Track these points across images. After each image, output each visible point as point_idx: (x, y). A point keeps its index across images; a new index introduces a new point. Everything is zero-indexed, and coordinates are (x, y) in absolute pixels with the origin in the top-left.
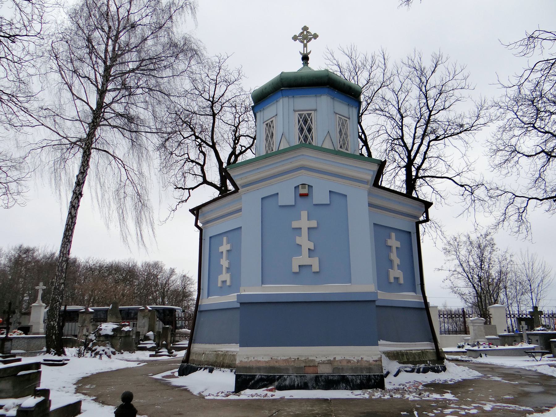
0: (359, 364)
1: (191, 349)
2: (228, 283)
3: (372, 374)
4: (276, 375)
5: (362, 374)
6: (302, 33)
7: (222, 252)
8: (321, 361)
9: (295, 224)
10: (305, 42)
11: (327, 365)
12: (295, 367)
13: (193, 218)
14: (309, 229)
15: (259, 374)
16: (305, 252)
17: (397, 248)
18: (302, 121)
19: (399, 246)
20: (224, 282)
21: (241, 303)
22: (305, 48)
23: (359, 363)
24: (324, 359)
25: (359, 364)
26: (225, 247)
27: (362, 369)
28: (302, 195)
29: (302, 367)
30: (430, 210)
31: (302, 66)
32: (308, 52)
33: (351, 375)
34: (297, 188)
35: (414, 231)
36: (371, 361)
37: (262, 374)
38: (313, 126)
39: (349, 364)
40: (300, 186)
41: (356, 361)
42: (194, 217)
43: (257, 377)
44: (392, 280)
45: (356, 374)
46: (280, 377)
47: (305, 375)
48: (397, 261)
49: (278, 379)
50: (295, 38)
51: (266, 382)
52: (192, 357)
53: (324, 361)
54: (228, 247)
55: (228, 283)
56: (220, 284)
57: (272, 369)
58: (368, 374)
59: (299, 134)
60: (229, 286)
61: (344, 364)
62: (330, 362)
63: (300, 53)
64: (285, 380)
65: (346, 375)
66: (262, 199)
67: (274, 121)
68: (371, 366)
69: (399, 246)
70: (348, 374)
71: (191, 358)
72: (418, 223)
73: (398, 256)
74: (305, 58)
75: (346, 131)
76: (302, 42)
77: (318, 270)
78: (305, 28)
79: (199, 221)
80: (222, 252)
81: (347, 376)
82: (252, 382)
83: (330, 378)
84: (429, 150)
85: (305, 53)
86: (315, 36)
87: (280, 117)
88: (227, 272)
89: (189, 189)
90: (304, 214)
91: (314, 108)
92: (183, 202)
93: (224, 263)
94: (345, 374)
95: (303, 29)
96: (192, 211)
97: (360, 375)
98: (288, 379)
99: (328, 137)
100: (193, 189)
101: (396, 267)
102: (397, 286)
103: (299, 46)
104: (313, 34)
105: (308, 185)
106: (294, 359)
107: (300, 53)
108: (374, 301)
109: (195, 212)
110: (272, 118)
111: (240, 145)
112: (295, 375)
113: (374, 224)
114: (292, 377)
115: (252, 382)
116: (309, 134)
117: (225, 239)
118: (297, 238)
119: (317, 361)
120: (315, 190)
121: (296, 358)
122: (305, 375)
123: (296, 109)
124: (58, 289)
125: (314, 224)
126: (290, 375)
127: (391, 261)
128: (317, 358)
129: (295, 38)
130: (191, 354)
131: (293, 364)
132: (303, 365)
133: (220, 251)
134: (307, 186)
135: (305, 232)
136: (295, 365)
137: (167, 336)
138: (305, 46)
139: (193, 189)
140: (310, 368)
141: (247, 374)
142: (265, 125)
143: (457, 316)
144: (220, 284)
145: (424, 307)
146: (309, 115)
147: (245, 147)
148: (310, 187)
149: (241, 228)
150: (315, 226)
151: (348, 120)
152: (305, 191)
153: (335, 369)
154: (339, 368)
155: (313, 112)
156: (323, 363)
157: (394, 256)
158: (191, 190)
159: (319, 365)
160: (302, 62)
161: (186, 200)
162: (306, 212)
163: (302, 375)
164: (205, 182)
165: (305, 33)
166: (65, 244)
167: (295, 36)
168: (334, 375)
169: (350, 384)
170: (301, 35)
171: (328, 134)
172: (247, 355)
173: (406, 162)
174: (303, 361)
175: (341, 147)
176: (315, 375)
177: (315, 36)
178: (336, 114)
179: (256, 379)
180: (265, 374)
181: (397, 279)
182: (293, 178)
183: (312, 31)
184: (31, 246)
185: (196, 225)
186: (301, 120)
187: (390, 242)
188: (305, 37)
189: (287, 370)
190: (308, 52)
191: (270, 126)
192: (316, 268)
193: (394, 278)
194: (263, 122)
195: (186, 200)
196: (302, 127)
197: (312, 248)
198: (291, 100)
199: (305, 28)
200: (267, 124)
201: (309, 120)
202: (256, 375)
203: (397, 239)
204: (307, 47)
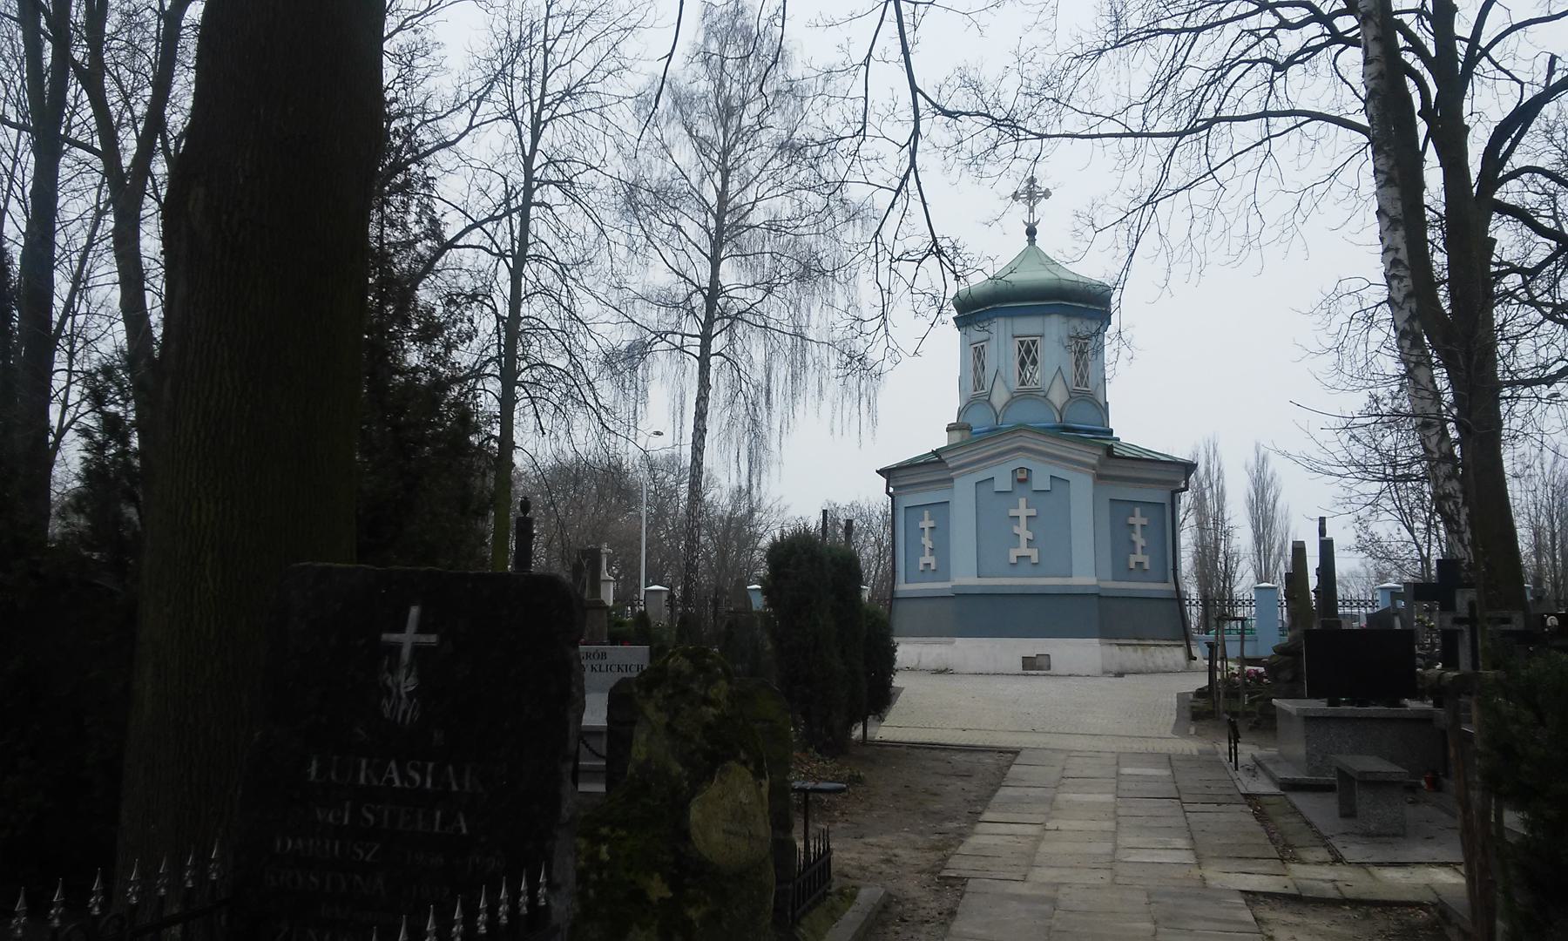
2: (933, 567)
9: (1013, 513)
16: (1024, 543)
22: (1031, 214)
26: (926, 524)
28: (1020, 481)
34: (1014, 471)
35: (1167, 501)
38: (1038, 359)
48: (1140, 541)
54: (932, 524)
55: (933, 567)
56: (921, 568)
60: (935, 570)
66: (976, 483)
77: (1037, 561)
85: (1031, 222)
90: (1022, 502)
93: (927, 542)
99: (1059, 376)
101: (1139, 550)
102: (1140, 571)
103: (1021, 208)
117: (926, 513)
123: (1016, 333)
124: (692, 565)
125: (1033, 512)
127: (1133, 543)
133: (921, 527)
135: (1023, 521)
138: (1031, 210)
143: (1347, 604)
145: (1176, 597)
146: (1034, 342)
149: (948, 502)
150: (1035, 514)
152: (1023, 476)
162: (1024, 499)
166: (694, 504)
171: (1059, 372)
175: (1077, 385)
181: (1139, 564)
185: (888, 492)
187: (1131, 520)
192: (1035, 559)
193: (1136, 563)
197: (1031, 538)
198: (1009, 321)
203: (1142, 516)
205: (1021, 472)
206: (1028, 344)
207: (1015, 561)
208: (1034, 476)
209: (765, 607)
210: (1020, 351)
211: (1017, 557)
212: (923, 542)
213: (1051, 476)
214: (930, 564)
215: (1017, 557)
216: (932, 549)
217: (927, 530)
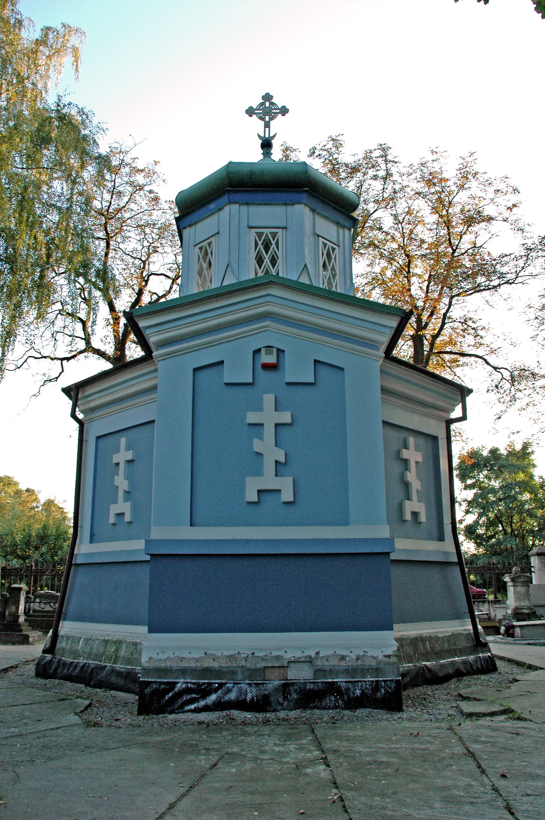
0: (360, 662)
1: (59, 629)
2: (127, 518)
3: (382, 679)
4: (213, 683)
5: (364, 680)
6: (262, 104)
7: (117, 464)
8: (293, 659)
9: (252, 417)
10: (267, 118)
11: (305, 664)
12: (249, 669)
13: (68, 403)
14: (277, 425)
15: (182, 680)
16: (269, 467)
17: (417, 463)
18: (262, 244)
19: (420, 459)
20: (121, 515)
21: (152, 555)
22: (267, 129)
23: (359, 661)
24: (298, 654)
25: (360, 662)
27: (364, 671)
28: (267, 367)
29: (260, 669)
30: (469, 399)
31: (262, 157)
32: (271, 136)
33: (345, 682)
34: (257, 352)
36: (380, 657)
37: (188, 680)
39: (343, 663)
40: (263, 351)
41: (355, 658)
42: (71, 402)
43: (179, 685)
44: (408, 517)
45: (355, 680)
46: (221, 685)
47: (265, 682)
49: (216, 690)
50: (250, 112)
51: (194, 696)
52: (61, 644)
53: (300, 658)
54: (129, 455)
55: (127, 518)
56: (112, 520)
57: (207, 672)
58: (375, 679)
59: (255, 267)
60: (130, 523)
61: (334, 662)
62: (310, 661)
63: (259, 136)
64: (229, 691)
65: (337, 682)
66: (195, 370)
67: (213, 244)
68: (380, 666)
69: (420, 459)
70: (340, 680)
71: (58, 646)
72: (450, 422)
73: (419, 477)
74: (267, 145)
75: (333, 266)
76: (262, 119)
77: (291, 499)
78: (267, 97)
79: (77, 409)
80: (117, 464)
81: (339, 684)
82: (170, 694)
83: (308, 688)
84: (450, 311)
85: (267, 136)
86: (284, 111)
87: (224, 235)
88: (126, 500)
89: (62, 360)
90: (269, 400)
91: (283, 224)
92: (50, 380)
94: (335, 680)
95: (263, 98)
96: (67, 391)
97: (360, 681)
98: (235, 689)
100: (68, 359)
104: (280, 107)
105: (278, 350)
106: (246, 655)
107: (259, 136)
108: (388, 553)
109: (72, 394)
110: (208, 238)
111: (150, 292)
112: (247, 682)
113: (384, 422)
114: (242, 685)
115: (170, 694)
116: (273, 267)
118: (256, 441)
119: (286, 658)
120: (287, 357)
121: (250, 653)
122: (265, 682)
123: (251, 224)
125: (286, 417)
126: (238, 682)
127: (407, 485)
128: (286, 652)
129: (250, 112)
130: (59, 638)
131: (243, 663)
132: (261, 665)
133: (115, 461)
134: (275, 350)
135: (269, 431)
136: (248, 666)
137: (19, 601)
138: (267, 125)
139: (68, 359)
140: (273, 670)
141: (161, 680)
142: (198, 250)
144: (112, 520)
146: (274, 235)
147: (157, 295)
148: (280, 352)
150: (289, 420)
151: (337, 247)
152: (271, 359)
153: (319, 672)
154: (325, 670)
155: (280, 231)
156: (298, 662)
157: (411, 477)
158: (65, 362)
159: (291, 664)
160: (262, 152)
161: (57, 378)
163: (259, 682)
164: (89, 348)
165: (267, 104)
167: (251, 108)
168: (315, 682)
169: (344, 697)
170: (260, 106)
172: (161, 648)
173: (415, 327)
174: (262, 659)
176: (283, 682)
177: (284, 111)
178: (318, 236)
179: (176, 689)
180: (193, 681)
181: (415, 514)
182: (251, 335)
183: (279, 101)
184: (18, 481)
185: (73, 415)
186: (260, 243)
187: (405, 454)
188: (267, 111)
189: (232, 673)
190: (271, 136)
191: (206, 251)
192: (287, 496)
194: (194, 245)
195: (57, 378)
196: (260, 256)
197: (283, 460)
199: (267, 97)
200: (201, 248)
201: (274, 243)
202: (177, 683)
203: (417, 449)
204: (269, 127)
205: (267, 353)
206: (267, 234)
207: (255, 499)
208: (288, 359)
209: (477, 534)
210: (256, 244)
211: (259, 491)
212: (116, 483)
213: (316, 361)
214: (123, 514)
215: (259, 491)
216: (129, 492)
217: (122, 467)
